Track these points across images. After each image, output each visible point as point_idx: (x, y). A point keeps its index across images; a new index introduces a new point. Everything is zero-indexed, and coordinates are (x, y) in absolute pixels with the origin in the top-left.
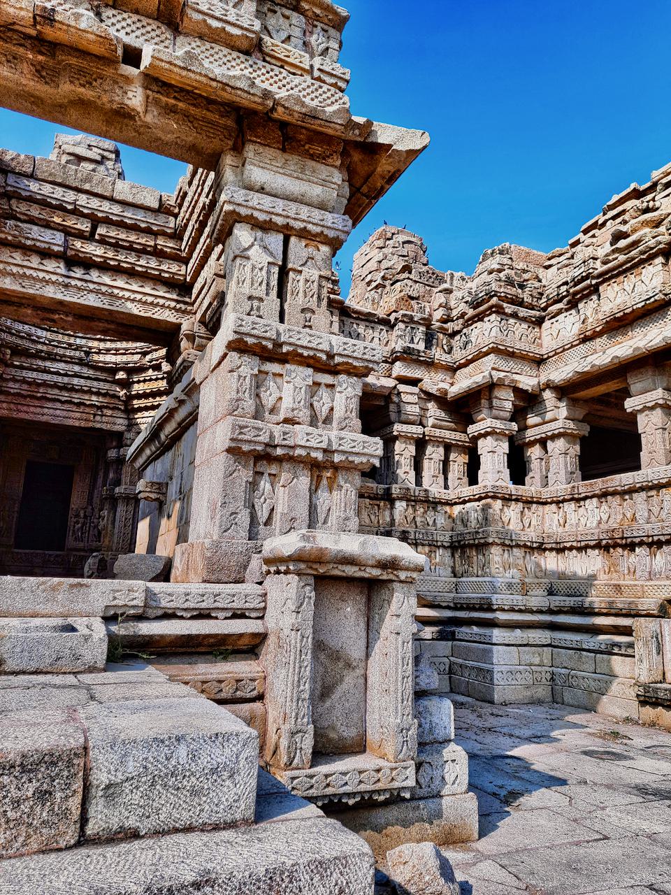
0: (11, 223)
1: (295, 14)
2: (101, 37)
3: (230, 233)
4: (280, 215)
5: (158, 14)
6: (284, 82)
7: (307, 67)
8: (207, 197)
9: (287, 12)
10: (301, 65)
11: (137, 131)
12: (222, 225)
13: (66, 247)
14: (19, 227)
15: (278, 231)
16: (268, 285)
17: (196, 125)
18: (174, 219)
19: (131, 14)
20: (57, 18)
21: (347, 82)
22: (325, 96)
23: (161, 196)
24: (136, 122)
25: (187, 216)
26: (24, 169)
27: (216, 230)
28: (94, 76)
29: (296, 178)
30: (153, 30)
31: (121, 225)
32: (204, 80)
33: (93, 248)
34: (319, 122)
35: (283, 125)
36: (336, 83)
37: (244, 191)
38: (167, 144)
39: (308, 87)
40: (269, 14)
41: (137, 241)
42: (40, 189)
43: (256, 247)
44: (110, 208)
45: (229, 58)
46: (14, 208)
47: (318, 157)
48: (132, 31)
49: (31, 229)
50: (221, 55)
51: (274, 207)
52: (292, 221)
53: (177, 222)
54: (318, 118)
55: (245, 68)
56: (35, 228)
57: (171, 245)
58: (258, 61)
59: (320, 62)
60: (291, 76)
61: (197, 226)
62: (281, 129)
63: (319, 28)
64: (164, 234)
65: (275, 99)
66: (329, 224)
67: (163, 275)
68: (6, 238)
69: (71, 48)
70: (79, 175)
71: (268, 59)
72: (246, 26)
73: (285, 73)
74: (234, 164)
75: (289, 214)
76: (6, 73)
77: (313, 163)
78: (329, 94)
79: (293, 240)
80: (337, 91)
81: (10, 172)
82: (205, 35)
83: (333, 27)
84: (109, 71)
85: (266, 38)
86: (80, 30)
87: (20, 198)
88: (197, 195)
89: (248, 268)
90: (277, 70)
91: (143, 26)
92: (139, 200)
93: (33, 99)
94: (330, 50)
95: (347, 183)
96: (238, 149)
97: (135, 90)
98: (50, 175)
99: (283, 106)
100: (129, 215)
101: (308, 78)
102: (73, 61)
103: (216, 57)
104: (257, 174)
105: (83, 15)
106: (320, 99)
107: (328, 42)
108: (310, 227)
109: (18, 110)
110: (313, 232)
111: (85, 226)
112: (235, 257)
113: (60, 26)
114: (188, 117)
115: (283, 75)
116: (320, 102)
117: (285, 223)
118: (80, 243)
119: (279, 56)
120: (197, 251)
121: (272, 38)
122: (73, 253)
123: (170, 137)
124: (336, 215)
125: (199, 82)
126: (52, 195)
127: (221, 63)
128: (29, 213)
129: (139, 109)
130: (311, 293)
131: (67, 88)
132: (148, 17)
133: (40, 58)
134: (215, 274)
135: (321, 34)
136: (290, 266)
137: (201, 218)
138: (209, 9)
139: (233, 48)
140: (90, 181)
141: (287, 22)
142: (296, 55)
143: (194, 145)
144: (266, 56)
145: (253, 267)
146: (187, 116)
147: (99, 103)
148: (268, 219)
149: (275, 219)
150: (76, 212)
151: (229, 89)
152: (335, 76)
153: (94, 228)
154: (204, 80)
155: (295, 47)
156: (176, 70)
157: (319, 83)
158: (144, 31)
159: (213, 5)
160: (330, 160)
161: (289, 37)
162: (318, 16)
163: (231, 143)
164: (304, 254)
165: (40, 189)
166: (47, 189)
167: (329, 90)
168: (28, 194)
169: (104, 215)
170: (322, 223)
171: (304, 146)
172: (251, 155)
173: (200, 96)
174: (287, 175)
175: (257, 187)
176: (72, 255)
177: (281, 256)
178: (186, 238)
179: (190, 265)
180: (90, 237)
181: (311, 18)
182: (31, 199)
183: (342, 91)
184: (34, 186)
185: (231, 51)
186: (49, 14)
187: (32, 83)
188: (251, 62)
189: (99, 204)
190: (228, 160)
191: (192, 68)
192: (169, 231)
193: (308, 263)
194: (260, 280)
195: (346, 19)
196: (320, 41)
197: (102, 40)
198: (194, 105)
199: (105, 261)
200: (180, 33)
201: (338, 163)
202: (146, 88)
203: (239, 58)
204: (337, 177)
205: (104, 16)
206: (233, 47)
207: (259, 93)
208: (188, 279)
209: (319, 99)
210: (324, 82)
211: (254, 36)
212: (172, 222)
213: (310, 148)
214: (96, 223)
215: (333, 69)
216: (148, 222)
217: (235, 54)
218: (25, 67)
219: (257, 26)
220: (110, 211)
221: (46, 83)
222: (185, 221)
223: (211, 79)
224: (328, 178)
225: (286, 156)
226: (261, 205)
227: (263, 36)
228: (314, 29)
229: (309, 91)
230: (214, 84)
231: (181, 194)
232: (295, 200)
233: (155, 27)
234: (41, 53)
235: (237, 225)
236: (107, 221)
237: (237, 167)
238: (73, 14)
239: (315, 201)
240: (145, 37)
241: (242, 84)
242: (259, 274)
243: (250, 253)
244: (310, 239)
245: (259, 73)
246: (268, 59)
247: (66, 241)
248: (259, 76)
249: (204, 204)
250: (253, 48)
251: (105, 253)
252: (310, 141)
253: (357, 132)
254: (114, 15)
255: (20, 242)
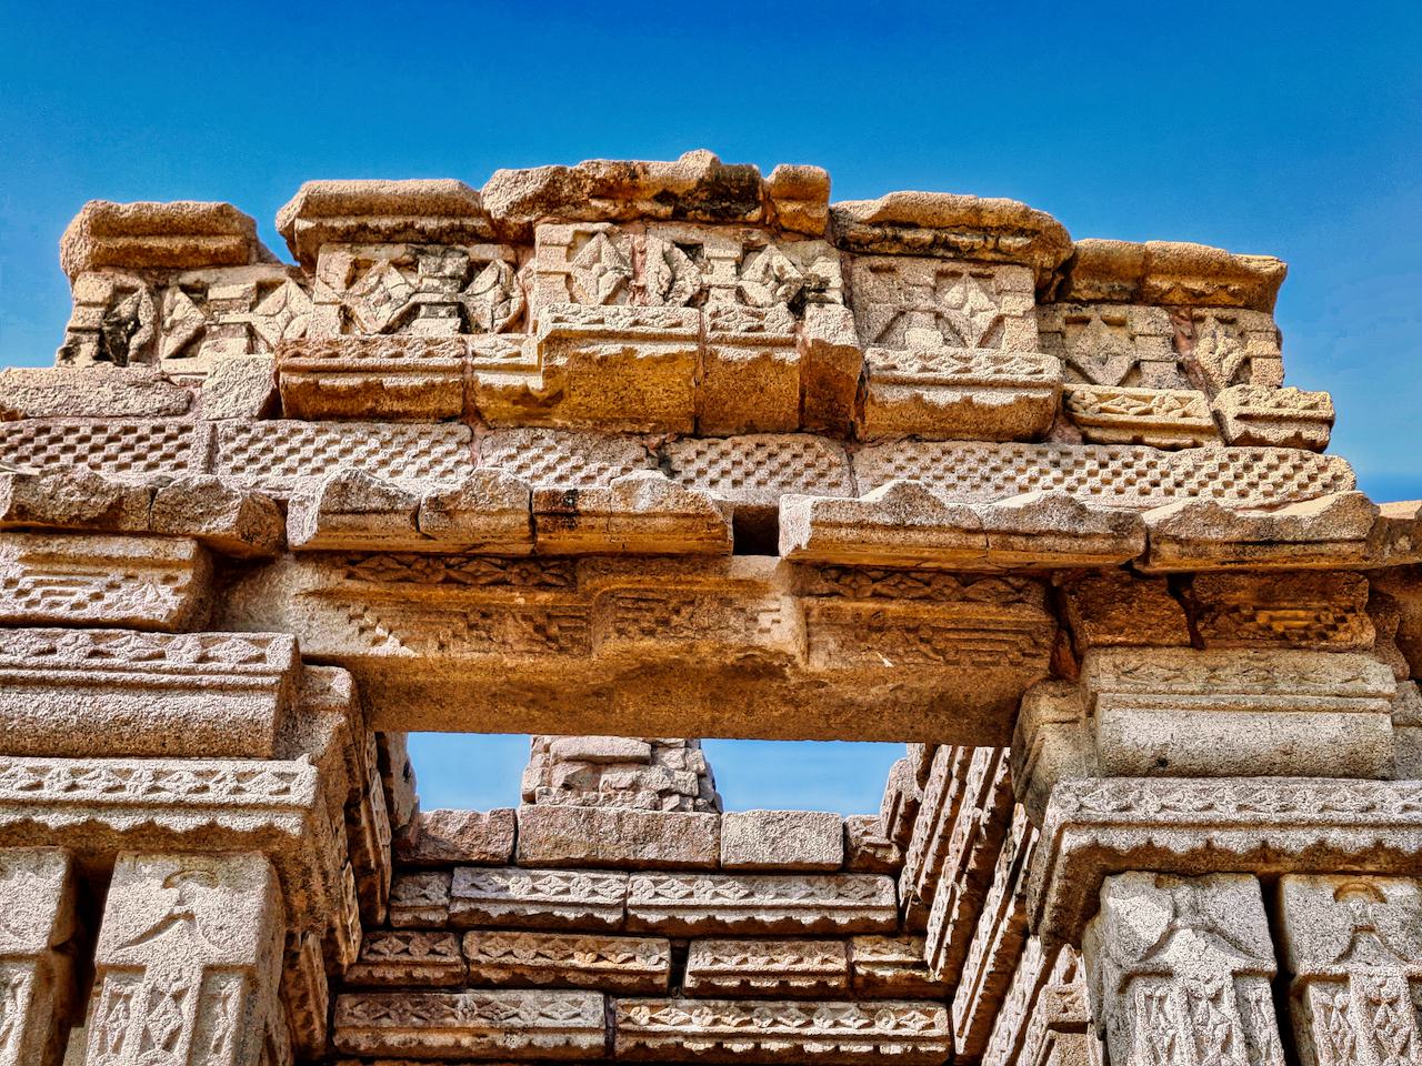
0: (467, 998)
1: (1139, 310)
2: (686, 516)
3: (1093, 907)
4: (1235, 825)
5: (802, 418)
6: (1154, 474)
7: (1207, 422)
8: (981, 804)
9: (1117, 312)
10: (1188, 421)
11: (791, 702)
12: (1065, 892)
13: (611, 1029)
14: (488, 1003)
15: (1238, 872)
16: (1249, 1043)
17: (941, 646)
18: (889, 881)
19: (738, 439)
20: (582, 508)
21: (1329, 422)
22: (1275, 476)
23: (845, 828)
24: (785, 678)
25: (928, 866)
26: (491, 849)
27: (1048, 909)
28: (674, 602)
29: (1255, 709)
30: (795, 456)
31: (750, 933)
32: (951, 539)
33: (683, 1016)
34: (1287, 550)
35: (1178, 583)
36: (1298, 435)
37: (1109, 785)
38: (870, 709)
39: (1223, 467)
40: (1072, 331)
41: (799, 967)
42: (535, 890)
43: (1183, 936)
44: (716, 894)
45: (994, 461)
46: (474, 955)
47: (1305, 637)
48: (748, 474)
49: (517, 1004)
50: (972, 461)
51: (1210, 807)
52: (1277, 834)
53: (902, 888)
54: (1284, 542)
55: (1042, 472)
56: (528, 997)
57: (894, 957)
58: (1072, 448)
59: (1238, 398)
60: (1169, 455)
61: (962, 888)
62: (1175, 592)
63: (1210, 321)
64: (868, 929)
65: (1148, 531)
66: (1396, 816)
67: (884, 1050)
68: (458, 1045)
69: (613, 555)
70: (628, 828)
71: (1094, 434)
72: (1022, 377)
73: (1148, 454)
74: (1063, 716)
75: (1263, 816)
76: (468, 656)
77: (1295, 658)
78: (1286, 468)
79: (1292, 888)
80: (1307, 453)
81: (459, 864)
82: (923, 429)
83: (1247, 307)
84: (708, 582)
85: (1079, 388)
86: (637, 516)
87: (487, 926)
88: (948, 803)
89: (1174, 1007)
90: (1126, 453)
91: (771, 456)
92: (790, 853)
93: (530, 695)
94: (1254, 363)
95: (1411, 684)
96: (1065, 672)
97: (774, 606)
98: (557, 846)
99: (1176, 540)
100: (768, 900)
101: (1215, 445)
102: (620, 583)
103: (961, 469)
104: (1139, 729)
105: (639, 483)
106: (1264, 486)
107: (1244, 346)
108: (1334, 837)
109: (498, 728)
110: (1352, 851)
111: (653, 960)
112: (1127, 981)
113: (590, 521)
114: (915, 630)
115: (1145, 460)
116: (1267, 494)
117: (1255, 844)
118: (645, 1010)
119: (1122, 418)
120: (974, 958)
121: (1093, 382)
122: (630, 1043)
123: (877, 693)
124: (1408, 785)
125: (939, 546)
126: (565, 898)
127: (977, 480)
128: (510, 960)
129: (792, 649)
130: (1398, 1041)
131: (611, 647)
132: (780, 431)
133: (543, 597)
134: (1052, 1026)
135: (1219, 334)
136: (1304, 967)
137: (972, 865)
138: (924, 369)
139: (999, 437)
140: (657, 836)
141: (1122, 334)
142: (1167, 401)
143: (942, 697)
144: (1089, 431)
145: (1191, 999)
146: (912, 629)
147: (691, 660)
148: (1200, 844)
149: (1222, 839)
150: (630, 928)
151: (1019, 542)
152: (1290, 419)
153: (679, 960)
154: (951, 539)
155: (1159, 385)
156: (876, 536)
157: (1248, 451)
158: (774, 465)
159: (932, 358)
160: (1341, 636)
161: (1136, 367)
162: (1202, 294)
163: (1042, 664)
164: (1339, 920)
165: (535, 890)
166: (551, 885)
167: (1282, 458)
168: (505, 909)
169: (702, 916)
170: (1370, 818)
171: (1252, 618)
172: (1107, 681)
173: (940, 571)
174: (1224, 708)
175: (1145, 763)
176: (627, 1051)
177: (1267, 945)
178: (934, 928)
179: (959, 1004)
180: (670, 988)
181: (1182, 305)
182: (514, 924)
183: (1319, 448)
184: (517, 886)
185: (992, 446)
186: (566, 505)
187: (528, 660)
188: (1052, 456)
189: (686, 889)
190: (1045, 711)
191: (916, 521)
192: (881, 918)
193: (1361, 947)
194: (1220, 1034)
195: (1277, 279)
196: (1221, 349)
197: (688, 522)
198: (927, 598)
199: (719, 1045)
200: (861, 443)
201: (1369, 636)
202: (800, 593)
203: (1019, 454)
204: (1379, 676)
205: (677, 464)
206: (998, 434)
207: (1102, 529)
208: (960, 1046)
209: (1261, 488)
210: (1262, 442)
211: (1047, 394)
212: (886, 894)
213: (1272, 618)
214: (678, 944)
215: (1279, 405)
216: (819, 908)
217: (1007, 449)
218: (512, 630)
219: (1051, 368)
220: (717, 901)
221: (561, 650)
222: (923, 881)
223: (969, 531)
224: (1349, 687)
225: (1209, 658)
226: (1170, 810)
227: (1068, 386)
228: (1199, 327)
229: (1228, 475)
230: (979, 540)
231: (901, 809)
232: (1267, 770)
233: (798, 449)
234: (544, 586)
235: (1110, 882)
236: (713, 932)
237: (1074, 721)
238: (617, 488)
239: (1329, 756)
240: (780, 478)
241: (1055, 520)
242: (1215, 1017)
243: (1168, 957)
244: (1344, 873)
245: (1081, 473)
246: (1094, 434)
247: (610, 1012)
248: (1081, 481)
249: (975, 825)
250: (1054, 422)
251: (715, 1022)
252: (1266, 600)
253: (1404, 543)
254: (699, 454)
255: (493, 1044)
